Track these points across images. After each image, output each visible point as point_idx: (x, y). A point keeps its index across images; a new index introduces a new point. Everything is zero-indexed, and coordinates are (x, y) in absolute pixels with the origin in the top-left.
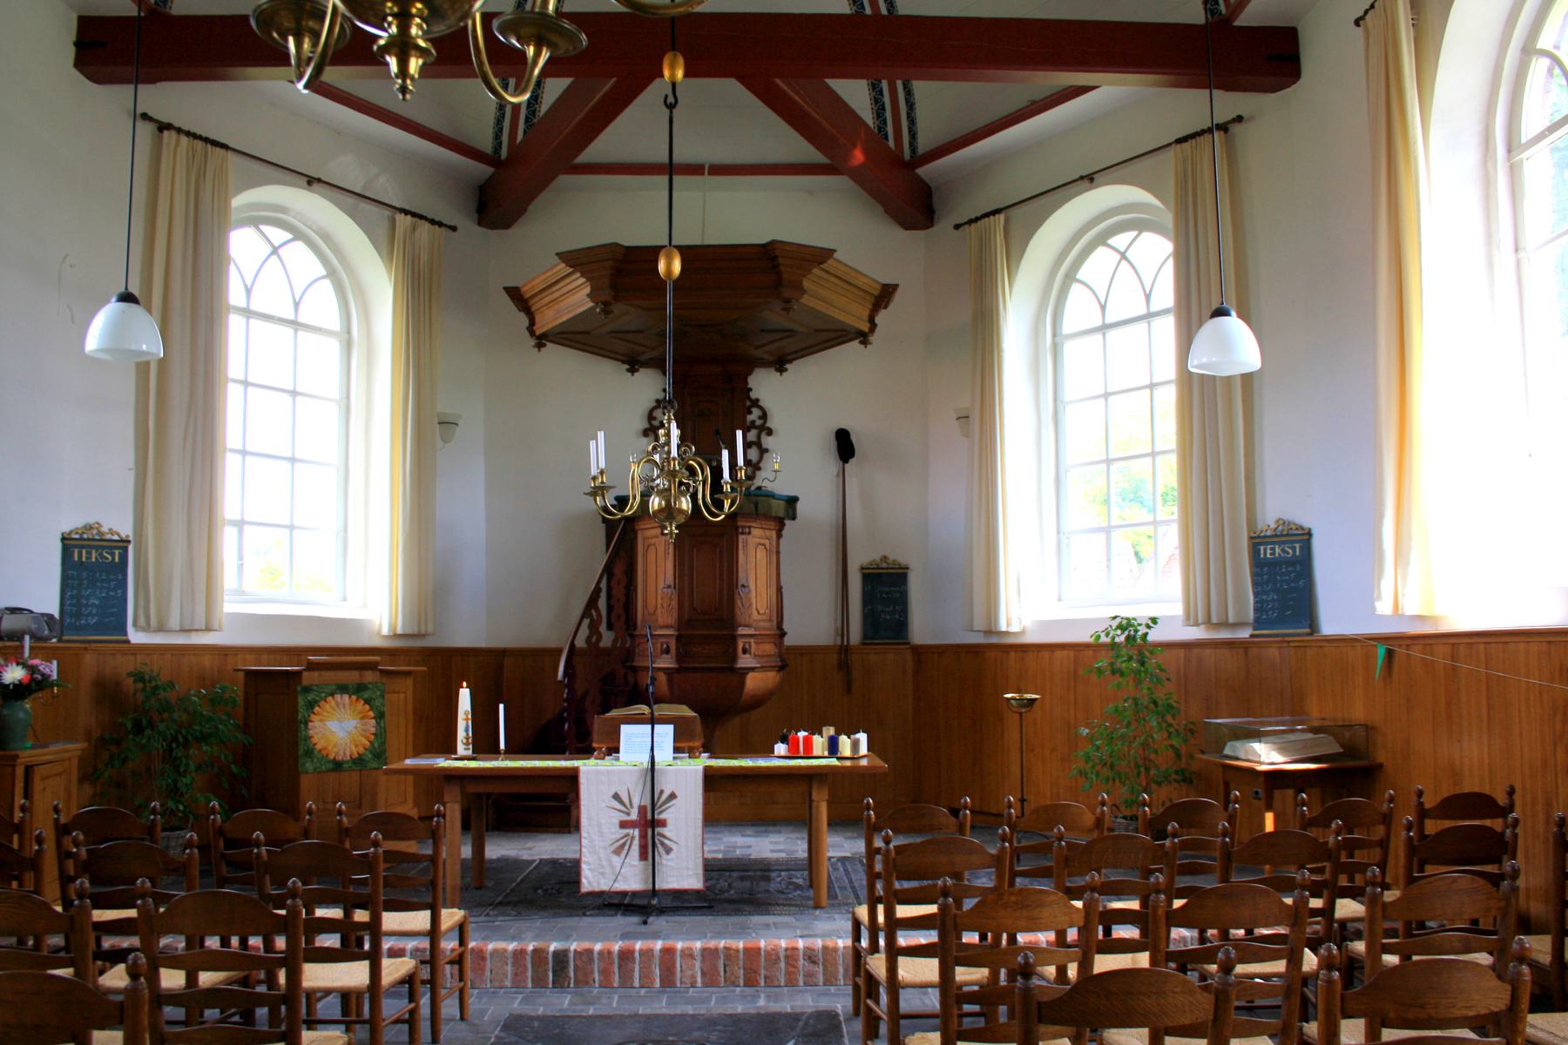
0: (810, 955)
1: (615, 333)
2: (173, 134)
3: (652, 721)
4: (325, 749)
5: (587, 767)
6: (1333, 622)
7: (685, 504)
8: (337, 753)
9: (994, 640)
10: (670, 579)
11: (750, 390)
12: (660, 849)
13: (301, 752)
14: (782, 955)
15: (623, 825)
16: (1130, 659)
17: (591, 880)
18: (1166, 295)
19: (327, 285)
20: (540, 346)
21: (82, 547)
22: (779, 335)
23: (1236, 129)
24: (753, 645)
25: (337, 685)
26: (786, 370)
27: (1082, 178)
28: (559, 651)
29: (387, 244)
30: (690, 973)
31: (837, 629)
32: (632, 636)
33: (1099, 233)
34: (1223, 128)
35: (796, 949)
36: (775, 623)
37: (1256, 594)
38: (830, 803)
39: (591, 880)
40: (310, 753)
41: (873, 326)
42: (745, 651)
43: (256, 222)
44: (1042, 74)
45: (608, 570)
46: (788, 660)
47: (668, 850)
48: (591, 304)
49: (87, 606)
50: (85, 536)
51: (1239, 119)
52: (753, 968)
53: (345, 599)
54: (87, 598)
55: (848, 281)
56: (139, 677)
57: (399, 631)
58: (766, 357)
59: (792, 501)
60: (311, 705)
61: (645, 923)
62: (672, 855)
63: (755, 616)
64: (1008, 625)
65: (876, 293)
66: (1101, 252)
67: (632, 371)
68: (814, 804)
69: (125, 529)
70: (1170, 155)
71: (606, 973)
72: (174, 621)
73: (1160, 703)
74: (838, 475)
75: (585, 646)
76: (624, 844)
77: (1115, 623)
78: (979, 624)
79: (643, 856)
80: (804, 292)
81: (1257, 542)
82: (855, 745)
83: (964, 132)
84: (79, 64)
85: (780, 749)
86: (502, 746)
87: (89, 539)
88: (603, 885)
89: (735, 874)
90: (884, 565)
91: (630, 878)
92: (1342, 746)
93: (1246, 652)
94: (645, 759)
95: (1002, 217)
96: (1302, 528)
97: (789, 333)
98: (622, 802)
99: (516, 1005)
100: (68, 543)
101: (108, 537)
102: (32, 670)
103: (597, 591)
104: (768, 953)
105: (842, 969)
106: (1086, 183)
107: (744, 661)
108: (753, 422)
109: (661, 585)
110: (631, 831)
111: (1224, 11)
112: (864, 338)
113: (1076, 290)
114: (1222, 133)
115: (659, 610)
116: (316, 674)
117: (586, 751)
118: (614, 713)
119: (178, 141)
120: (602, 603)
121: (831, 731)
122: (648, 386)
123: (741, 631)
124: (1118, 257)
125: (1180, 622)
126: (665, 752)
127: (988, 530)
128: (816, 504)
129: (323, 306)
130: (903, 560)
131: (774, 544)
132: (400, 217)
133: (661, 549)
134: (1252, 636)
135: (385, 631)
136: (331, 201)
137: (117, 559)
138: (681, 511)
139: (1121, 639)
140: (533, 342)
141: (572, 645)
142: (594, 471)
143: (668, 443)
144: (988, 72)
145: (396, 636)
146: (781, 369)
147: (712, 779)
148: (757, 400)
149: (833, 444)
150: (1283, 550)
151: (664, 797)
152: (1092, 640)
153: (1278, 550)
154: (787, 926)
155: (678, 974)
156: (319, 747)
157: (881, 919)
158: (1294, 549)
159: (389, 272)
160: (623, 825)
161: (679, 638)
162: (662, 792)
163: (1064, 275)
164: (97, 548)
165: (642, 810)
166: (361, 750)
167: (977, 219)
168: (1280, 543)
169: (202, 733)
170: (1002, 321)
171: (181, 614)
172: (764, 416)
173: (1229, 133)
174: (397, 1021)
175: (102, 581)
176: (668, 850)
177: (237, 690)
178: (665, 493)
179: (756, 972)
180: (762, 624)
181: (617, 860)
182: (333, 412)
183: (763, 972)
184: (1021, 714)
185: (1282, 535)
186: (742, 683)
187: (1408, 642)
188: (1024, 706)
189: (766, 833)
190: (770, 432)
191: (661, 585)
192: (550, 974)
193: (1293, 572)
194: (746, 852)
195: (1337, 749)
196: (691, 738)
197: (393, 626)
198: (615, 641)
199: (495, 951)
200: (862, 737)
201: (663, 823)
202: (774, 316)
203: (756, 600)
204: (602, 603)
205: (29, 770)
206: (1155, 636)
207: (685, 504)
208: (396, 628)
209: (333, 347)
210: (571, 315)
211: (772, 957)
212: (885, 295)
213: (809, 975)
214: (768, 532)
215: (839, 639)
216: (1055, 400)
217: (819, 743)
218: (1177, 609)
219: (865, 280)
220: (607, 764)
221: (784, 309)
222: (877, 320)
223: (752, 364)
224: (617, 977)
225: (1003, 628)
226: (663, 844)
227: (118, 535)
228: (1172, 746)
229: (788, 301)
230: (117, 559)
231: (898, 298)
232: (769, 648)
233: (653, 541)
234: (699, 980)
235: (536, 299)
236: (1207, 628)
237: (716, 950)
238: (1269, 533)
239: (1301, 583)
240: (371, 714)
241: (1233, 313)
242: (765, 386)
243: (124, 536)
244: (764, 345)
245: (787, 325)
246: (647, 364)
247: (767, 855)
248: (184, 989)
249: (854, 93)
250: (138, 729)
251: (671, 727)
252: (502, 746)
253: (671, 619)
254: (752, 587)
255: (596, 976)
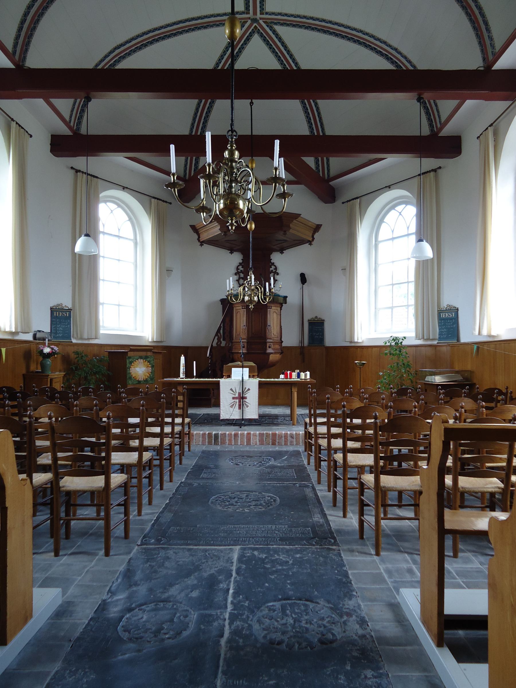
0: (292, 436)
1: (227, 241)
2: (81, 173)
3: (243, 367)
4: (135, 377)
5: (222, 381)
6: (465, 337)
7: (256, 299)
8: (139, 378)
9: (353, 345)
10: (245, 324)
11: (271, 259)
12: (245, 406)
13: (128, 378)
14: (283, 435)
15: (233, 398)
16: (396, 350)
17: (222, 417)
18: (413, 228)
19: (129, 223)
20: (201, 245)
21: (57, 311)
22: (283, 241)
23: (439, 171)
24: (272, 345)
25: (139, 356)
26: (284, 253)
27: (386, 187)
28: (208, 347)
29: (148, 209)
30: (255, 441)
31: (300, 341)
32: (232, 342)
33: (392, 205)
34: (435, 170)
35: (287, 434)
36: (279, 338)
37: (439, 329)
38: (298, 392)
39: (222, 417)
40: (130, 378)
41: (313, 239)
42: (269, 347)
43: (105, 202)
44: (372, 155)
45: (223, 321)
46: (284, 351)
47: (247, 406)
48: (220, 232)
49: (59, 330)
50: (57, 308)
51: (440, 168)
52: (274, 439)
53: (136, 330)
54: (59, 328)
55: (305, 224)
56: (77, 353)
57: (155, 340)
58: (276, 248)
59: (285, 297)
60: (131, 363)
61: (241, 428)
62: (248, 408)
63: (273, 336)
64: (358, 339)
65: (314, 227)
66: (393, 212)
67: (231, 253)
68: (293, 393)
69: (70, 306)
70: (416, 180)
71: (230, 440)
72: (86, 336)
73: (405, 364)
74: (301, 289)
75: (216, 346)
76: (234, 404)
77: (392, 339)
78: (348, 339)
79: (240, 408)
80: (290, 228)
81: (440, 312)
82: (306, 375)
83: (345, 170)
84: (52, 151)
85: (282, 376)
86: (195, 374)
87: (59, 309)
88: (227, 417)
89: (267, 418)
90: (316, 319)
91: (236, 415)
92: (463, 378)
93: (436, 349)
94: (241, 379)
95: (358, 200)
96: (455, 308)
97: (285, 241)
98: (233, 391)
99: (204, 448)
100: (53, 310)
101: (65, 308)
102: (52, 349)
103: (220, 327)
104: (279, 435)
105: (301, 440)
106: (387, 188)
107: (269, 351)
108: (272, 270)
109: (242, 325)
110: (236, 400)
111: (436, 130)
112: (310, 243)
113: (383, 225)
114: (434, 172)
115: (241, 334)
116: (132, 352)
117: (222, 377)
118: (230, 364)
119: (82, 175)
120: (221, 331)
121: (298, 371)
122: (237, 258)
123: (268, 340)
124: (399, 214)
125: (414, 339)
126: (246, 377)
127: (351, 307)
128: (293, 298)
129: (127, 230)
130: (323, 318)
131: (279, 312)
132: (153, 200)
133: (242, 313)
134: (437, 343)
135: (150, 340)
136: (127, 193)
137: (68, 315)
138: (254, 301)
139: (393, 344)
140: (199, 244)
141: (212, 345)
142: (228, 289)
143: (251, 280)
144: (354, 154)
145: (154, 342)
146: (282, 253)
147: (261, 384)
148: (274, 263)
149: (299, 278)
150: (449, 315)
151: (246, 390)
152: (383, 344)
153: (447, 315)
154: (284, 429)
155: (252, 441)
156: (133, 376)
157: (313, 421)
158: (452, 314)
159: (150, 218)
160: (233, 398)
161: (247, 343)
162: (245, 388)
163: (379, 220)
164: (61, 311)
165: (239, 393)
166: (147, 377)
167: (350, 201)
168: (447, 312)
169: (96, 371)
170: (357, 237)
171: (88, 333)
172: (276, 269)
173: (437, 172)
174: (119, 505)
175: (63, 322)
176: (247, 406)
177: (106, 357)
178: (250, 296)
179: (275, 441)
180: (275, 338)
181: (231, 409)
182: (132, 267)
183: (277, 441)
184: (360, 368)
185: (448, 310)
186: (269, 358)
187: (484, 344)
188: (361, 365)
189: (276, 408)
190: (278, 274)
191: (242, 325)
192: (213, 441)
193: (451, 322)
194: (269, 412)
195: (461, 378)
196: (254, 372)
197: (153, 338)
198: (226, 344)
199: (196, 434)
200: (308, 373)
201: (246, 398)
202: (280, 236)
203: (273, 331)
204: (221, 331)
205: (51, 380)
206: (405, 343)
207: (256, 299)
208: (154, 338)
209: (131, 244)
210: (213, 235)
211: (280, 436)
212: (318, 228)
213: (291, 442)
214: (277, 308)
215: (301, 344)
216: (375, 263)
217: (294, 375)
218: (413, 334)
219: (310, 223)
220: (228, 380)
221: (284, 234)
222: (315, 236)
223: (273, 251)
224: (233, 442)
225: (356, 341)
226: (246, 404)
227: (68, 307)
228: (410, 379)
229: (285, 231)
230: (68, 315)
231: (322, 228)
232: (277, 347)
233: (239, 310)
234: (258, 443)
235: (201, 229)
236: (423, 341)
237: (263, 434)
238: (444, 309)
239: (454, 326)
240: (150, 366)
241: (424, 241)
242: (276, 258)
243: (70, 308)
244: (276, 245)
245: (285, 239)
246: (236, 251)
247: (277, 413)
248: (120, 433)
249: (310, 161)
250: (76, 369)
251: (248, 369)
252: (195, 374)
253: (245, 337)
254: (272, 326)
255: (227, 441)
